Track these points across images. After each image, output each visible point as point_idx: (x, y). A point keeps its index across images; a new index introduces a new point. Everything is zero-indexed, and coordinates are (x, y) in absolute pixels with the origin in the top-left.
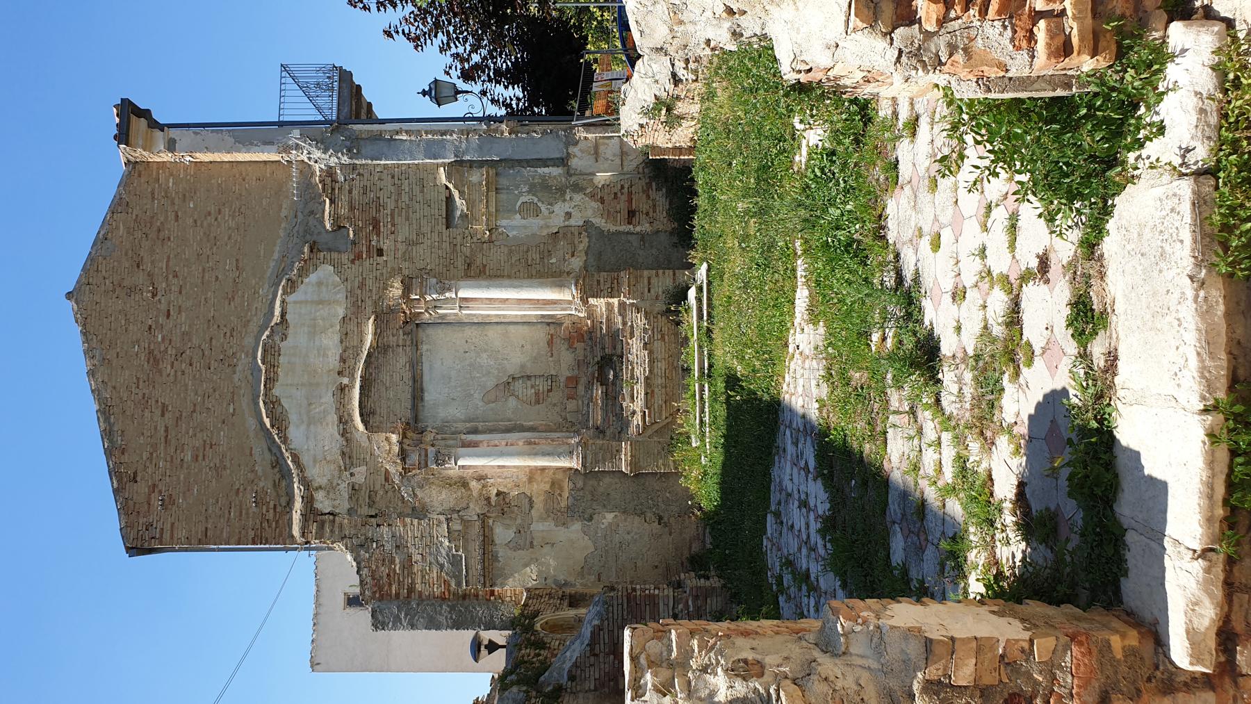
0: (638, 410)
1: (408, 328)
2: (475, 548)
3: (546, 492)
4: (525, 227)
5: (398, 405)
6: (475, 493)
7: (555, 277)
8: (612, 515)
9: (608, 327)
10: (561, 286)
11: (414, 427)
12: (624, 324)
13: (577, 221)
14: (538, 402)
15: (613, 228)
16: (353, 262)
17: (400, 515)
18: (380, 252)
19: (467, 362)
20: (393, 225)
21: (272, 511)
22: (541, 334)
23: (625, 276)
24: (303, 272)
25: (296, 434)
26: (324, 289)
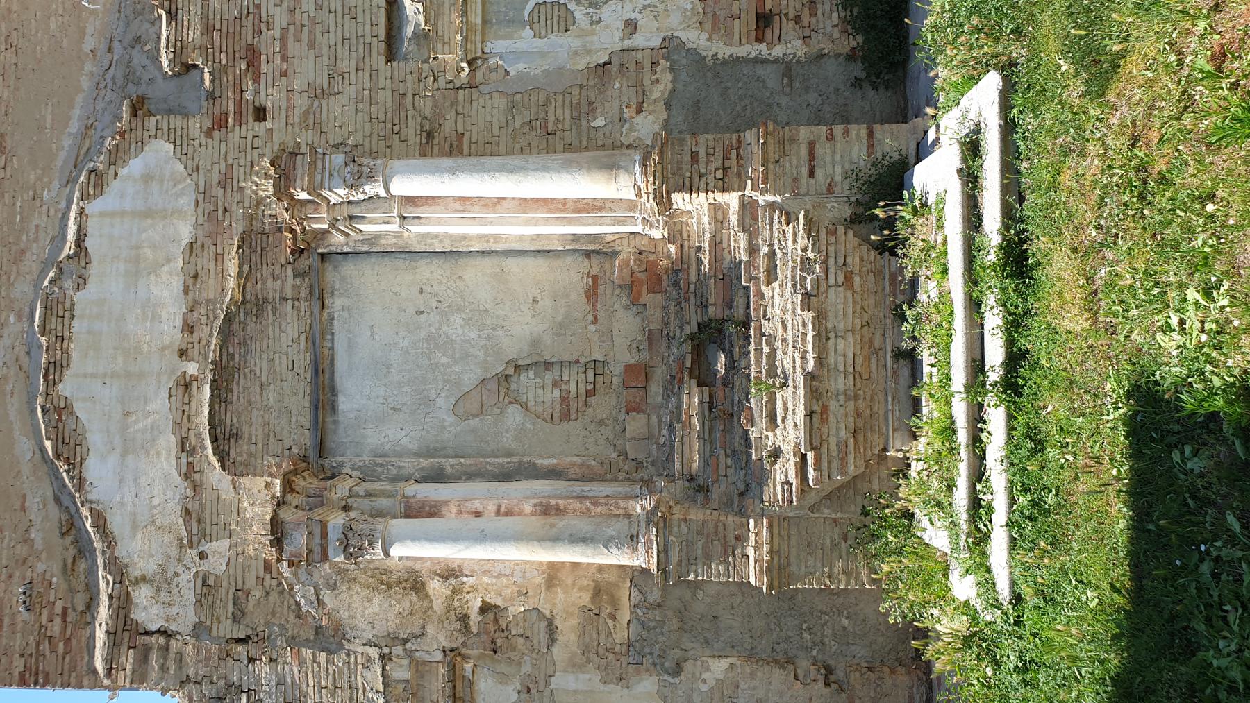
0: (788, 448)
1: (304, 262)
3: (583, 609)
4: (542, 54)
5: (284, 421)
6: (438, 605)
7: (603, 151)
8: (723, 664)
9: (715, 258)
10: (611, 167)
11: (315, 461)
12: (753, 250)
13: (648, 38)
14: (566, 416)
15: (724, 51)
16: (209, 133)
17: (293, 642)
18: (260, 114)
19: (423, 334)
20: (285, 59)
21: (58, 620)
22: (573, 275)
23: (754, 141)
24: (117, 157)
25: (100, 472)
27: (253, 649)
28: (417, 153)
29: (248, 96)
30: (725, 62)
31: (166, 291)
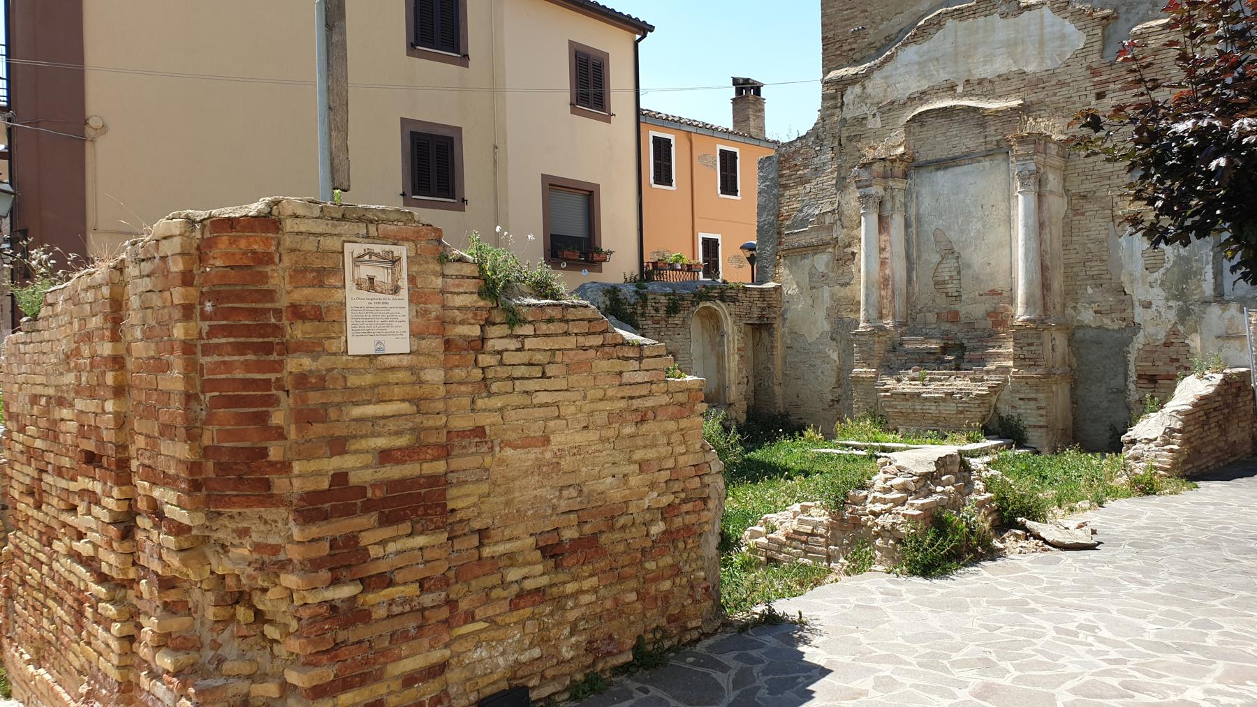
2: (813, 239)
4: (1131, 256)
5: (929, 147)
8: (836, 358)
9: (991, 354)
11: (912, 166)
12: (988, 372)
13: (1140, 315)
15: (1132, 357)
16: (1089, 68)
17: (840, 166)
22: (1000, 284)
25: (910, 54)
26: (1058, 43)
28: (487, 429)
29: (1112, 86)
30: (1125, 357)
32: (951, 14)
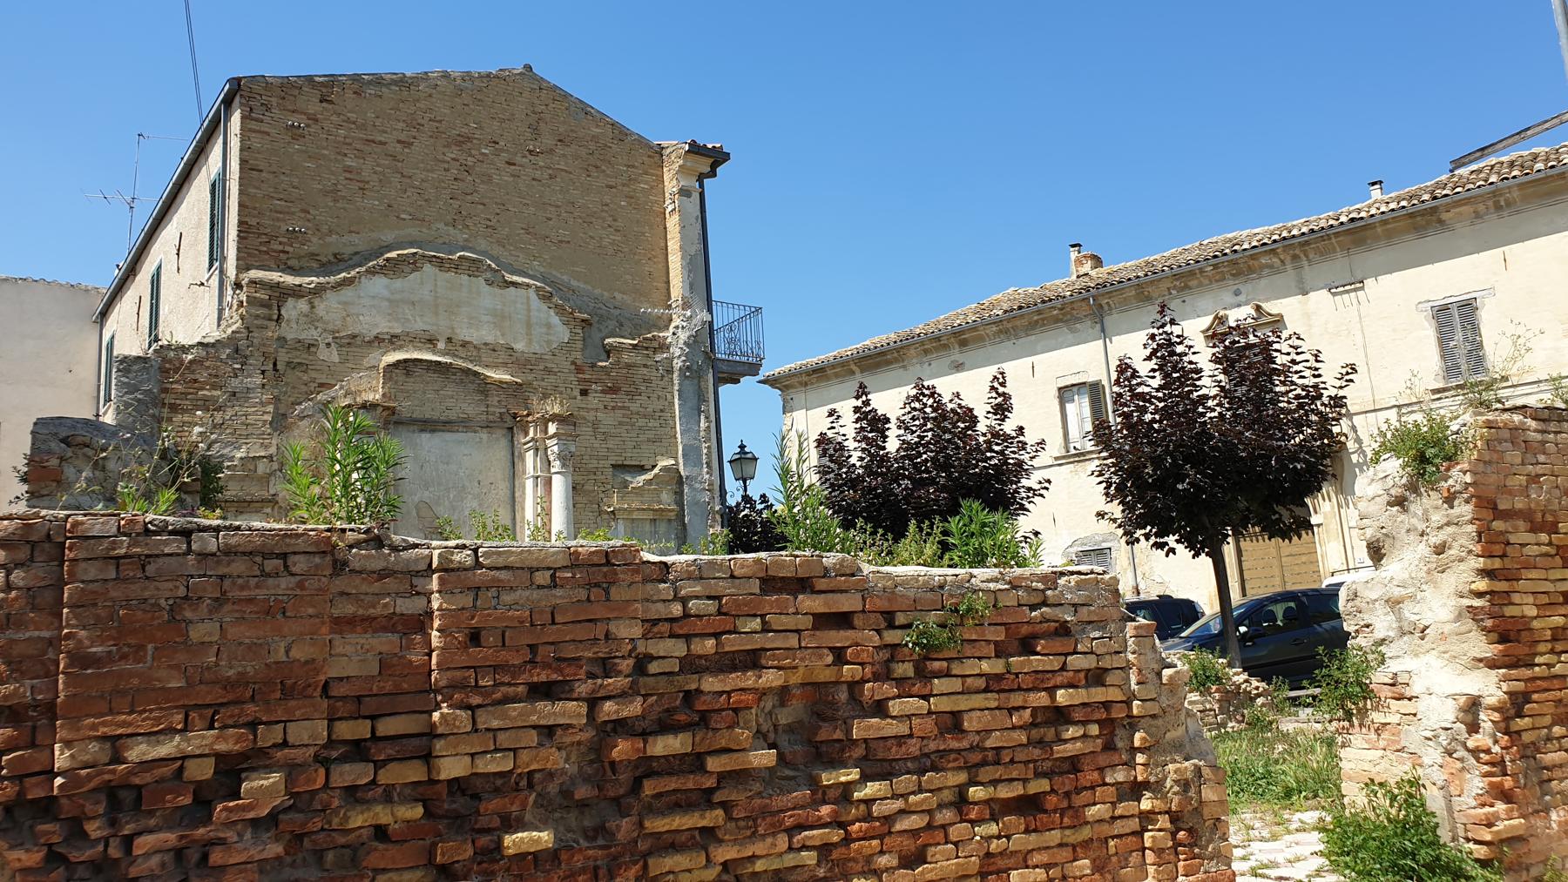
1: (508, 418)
17: (277, 400)
18: (584, 393)
20: (614, 408)
24: (560, 310)
27: (270, 373)
31: (484, 334)
32: (431, 259)
